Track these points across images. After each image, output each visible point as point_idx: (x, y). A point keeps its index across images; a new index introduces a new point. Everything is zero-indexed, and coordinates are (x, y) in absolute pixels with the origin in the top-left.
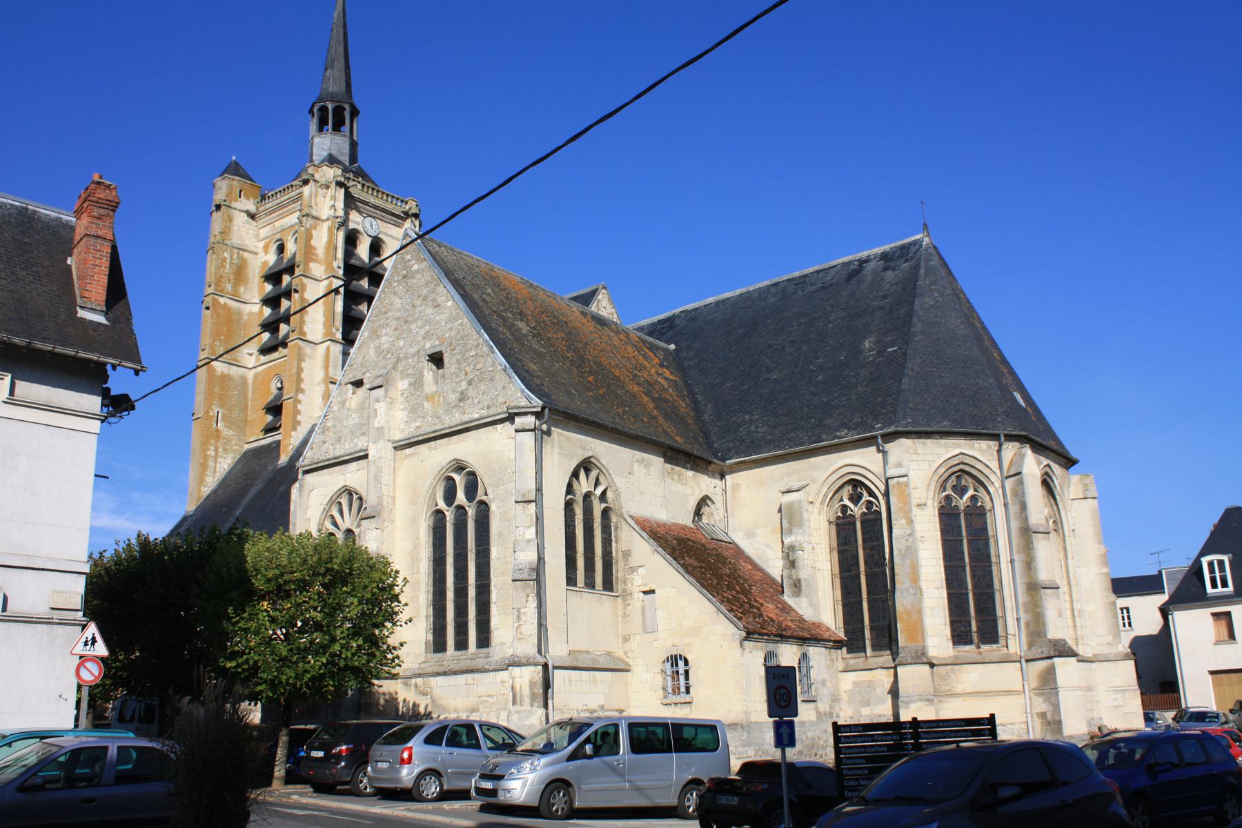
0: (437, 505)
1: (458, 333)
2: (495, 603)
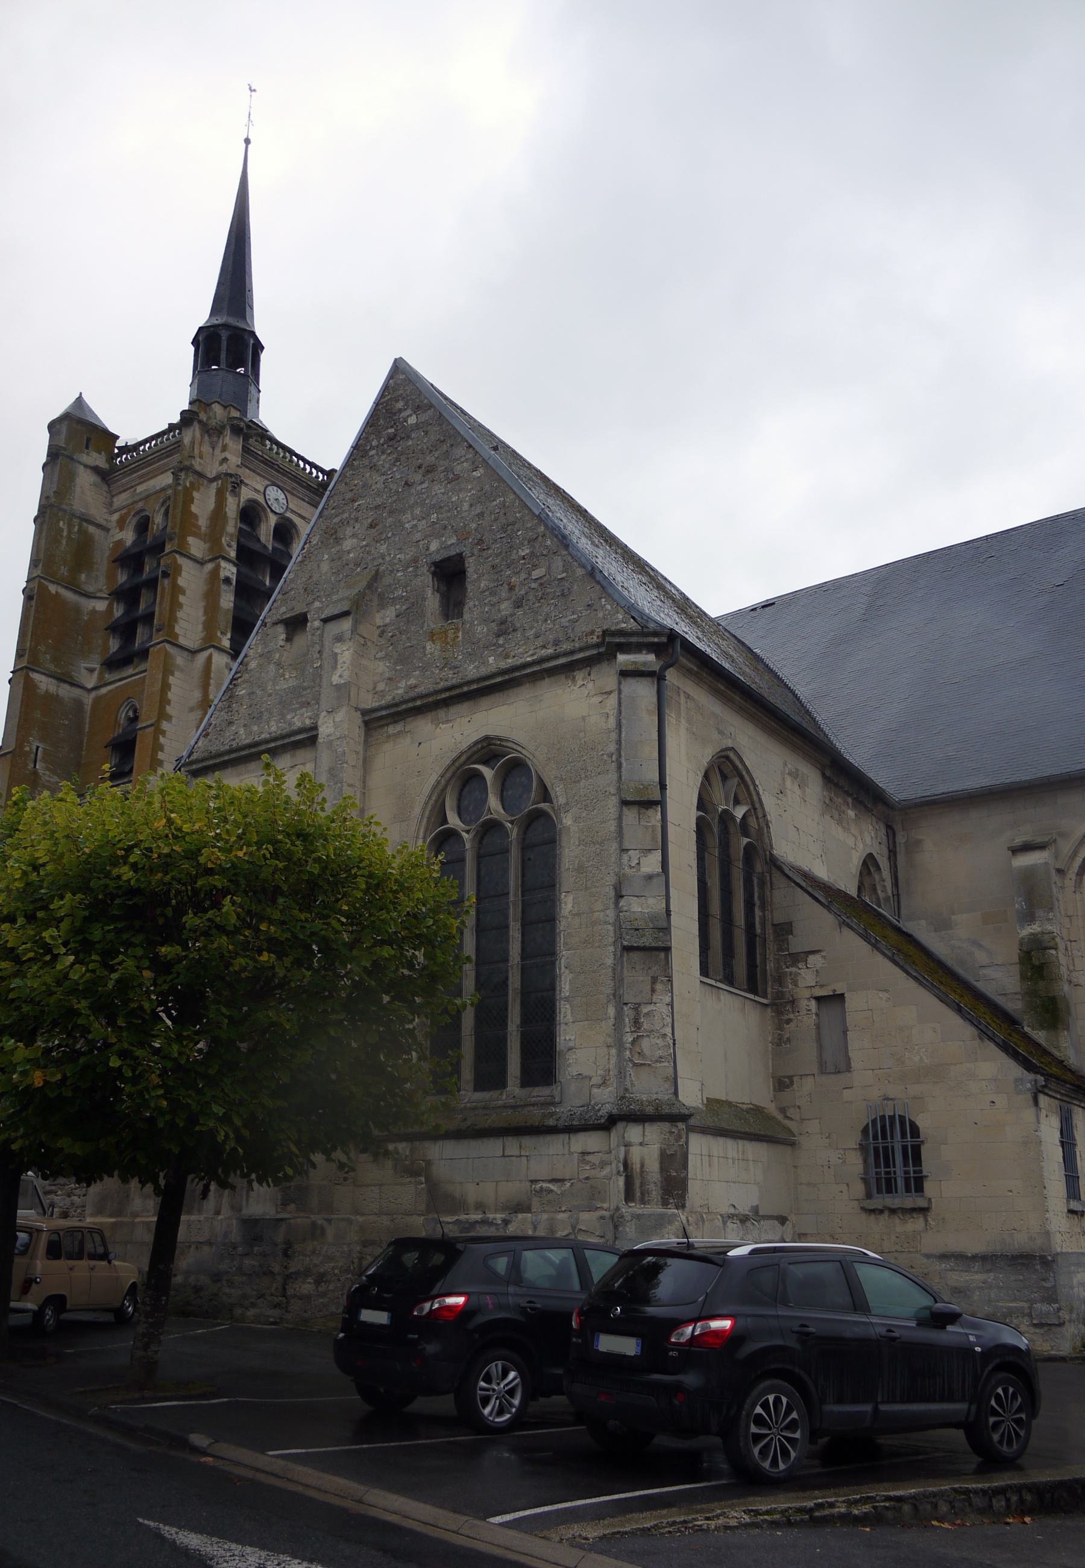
0: (445, 821)
1: (496, 520)
2: (567, 999)
